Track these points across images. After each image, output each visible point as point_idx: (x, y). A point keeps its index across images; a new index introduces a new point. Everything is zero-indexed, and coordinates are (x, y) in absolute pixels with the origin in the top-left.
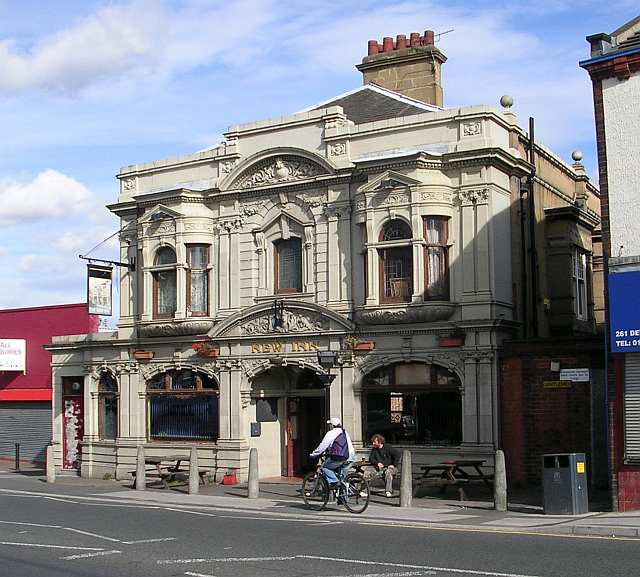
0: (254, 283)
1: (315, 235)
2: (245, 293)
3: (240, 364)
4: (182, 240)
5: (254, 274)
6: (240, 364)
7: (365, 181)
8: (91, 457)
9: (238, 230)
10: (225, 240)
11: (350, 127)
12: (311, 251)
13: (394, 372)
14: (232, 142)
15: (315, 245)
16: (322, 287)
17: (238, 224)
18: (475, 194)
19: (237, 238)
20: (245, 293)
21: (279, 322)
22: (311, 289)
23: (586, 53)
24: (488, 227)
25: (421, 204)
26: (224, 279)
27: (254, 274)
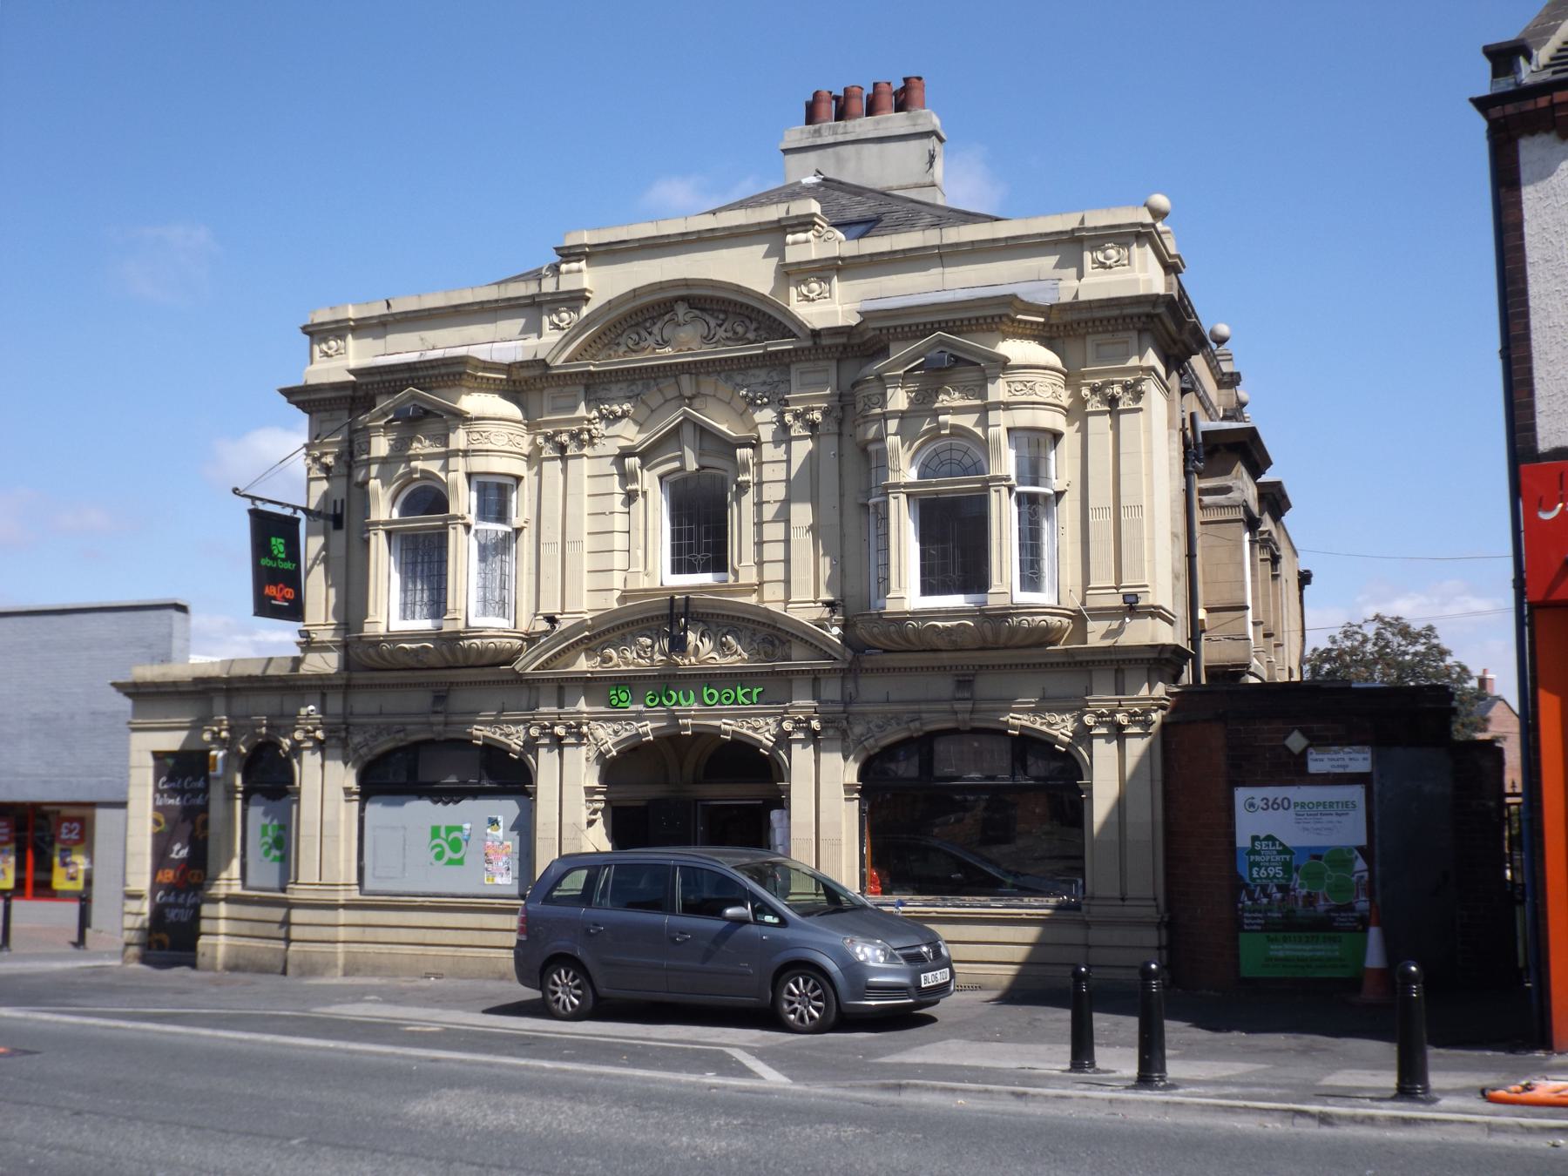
0: (619, 560)
1: (759, 464)
2: (601, 581)
3: (585, 729)
4: (1001, 422)
5: (619, 541)
6: (585, 729)
7: (883, 352)
8: (222, 926)
9: (586, 451)
10: (552, 469)
11: (838, 244)
12: (748, 500)
13: (931, 752)
14: (574, 266)
15: (760, 484)
16: (774, 572)
17: (586, 436)
18: (1117, 389)
19: (583, 468)
20: (601, 581)
21: (679, 645)
22: (748, 576)
23: (1482, 82)
24: (811, 458)
25: (1007, 406)
26: (551, 555)
27: (619, 541)
